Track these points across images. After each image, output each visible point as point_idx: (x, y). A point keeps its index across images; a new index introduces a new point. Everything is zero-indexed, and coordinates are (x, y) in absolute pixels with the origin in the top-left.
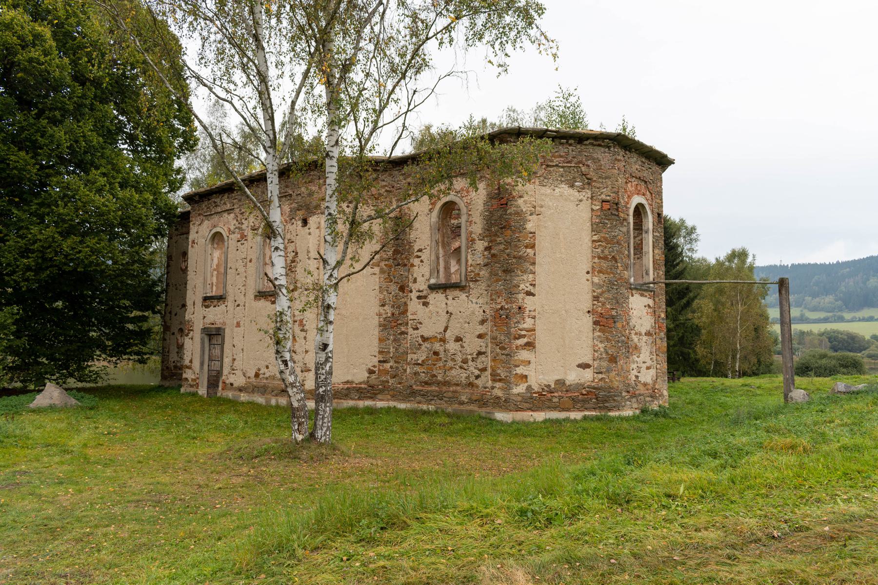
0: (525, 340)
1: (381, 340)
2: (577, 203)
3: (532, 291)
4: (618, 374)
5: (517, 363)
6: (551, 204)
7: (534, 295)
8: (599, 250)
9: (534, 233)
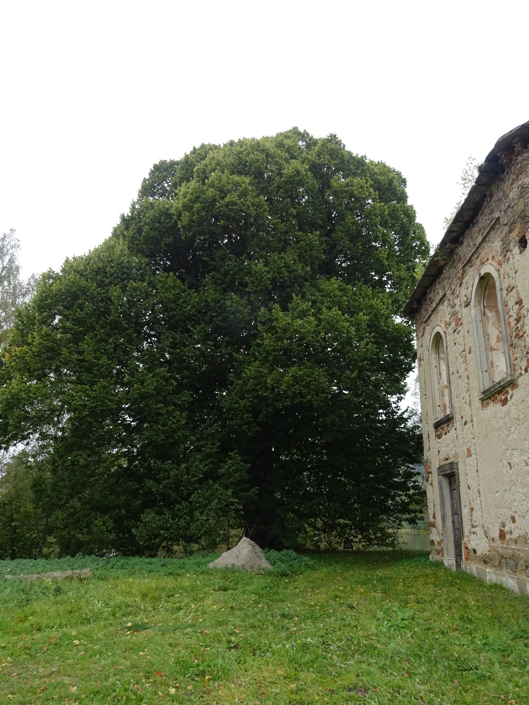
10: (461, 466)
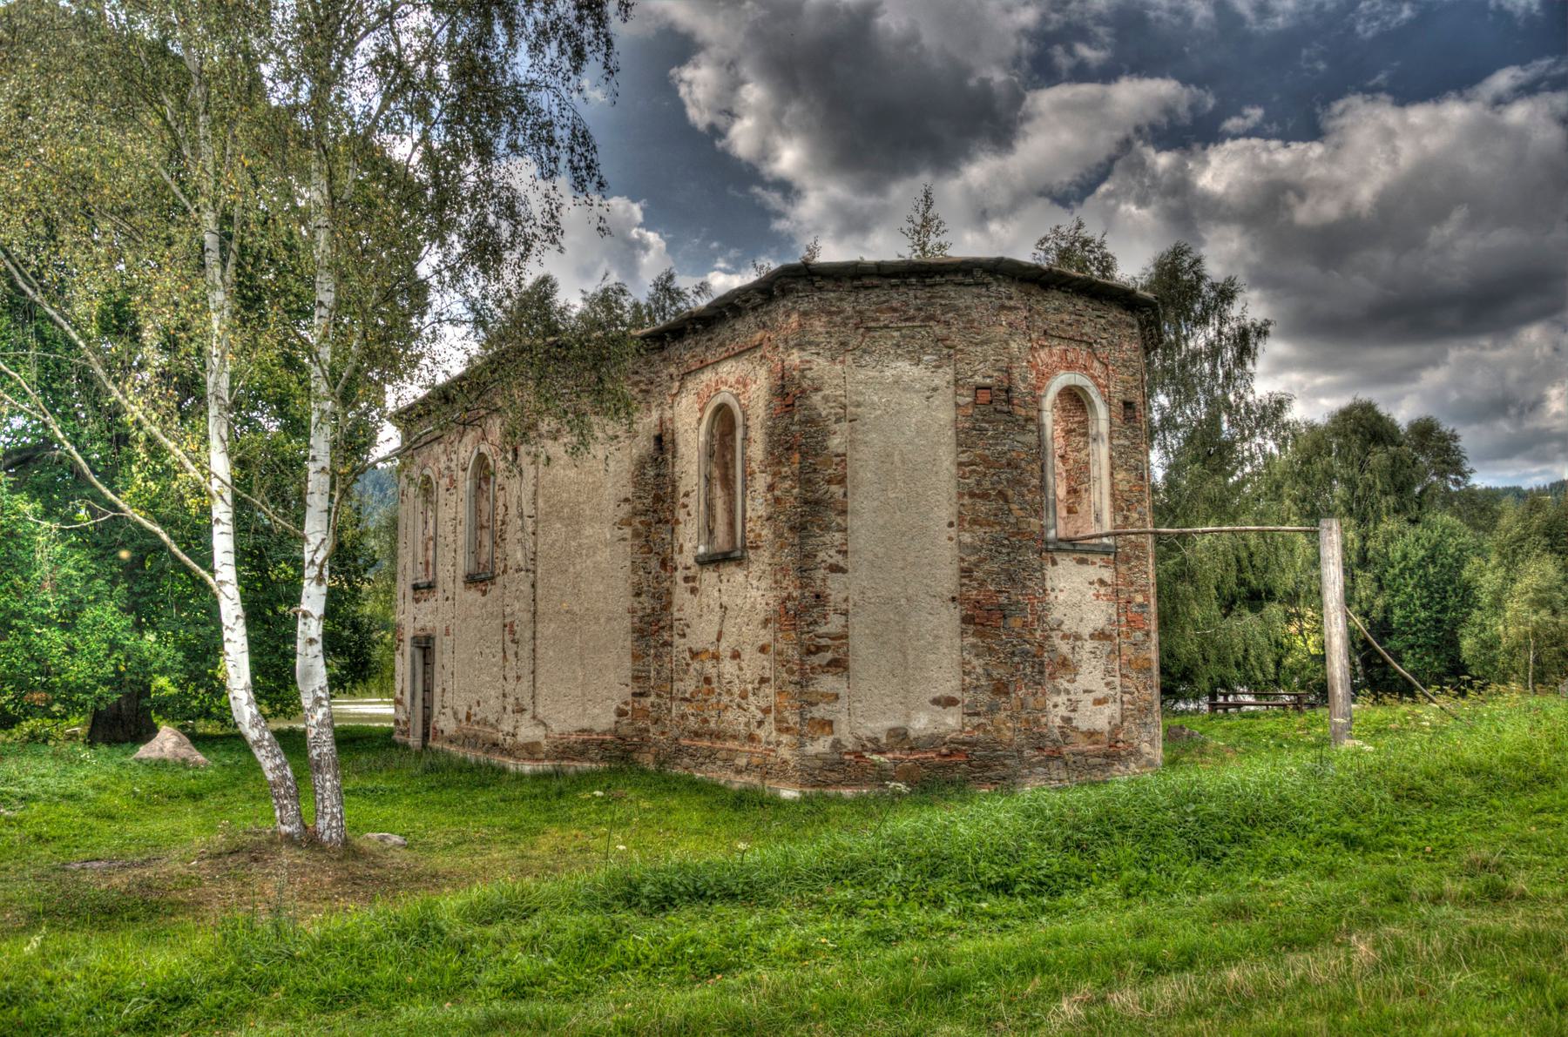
0: (829, 655)
1: (635, 657)
2: (928, 394)
3: (841, 564)
4: (1011, 717)
5: (813, 699)
6: (876, 399)
7: (843, 570)
8: (972, 481)
9: (844, 455)
10: (437, 642)
